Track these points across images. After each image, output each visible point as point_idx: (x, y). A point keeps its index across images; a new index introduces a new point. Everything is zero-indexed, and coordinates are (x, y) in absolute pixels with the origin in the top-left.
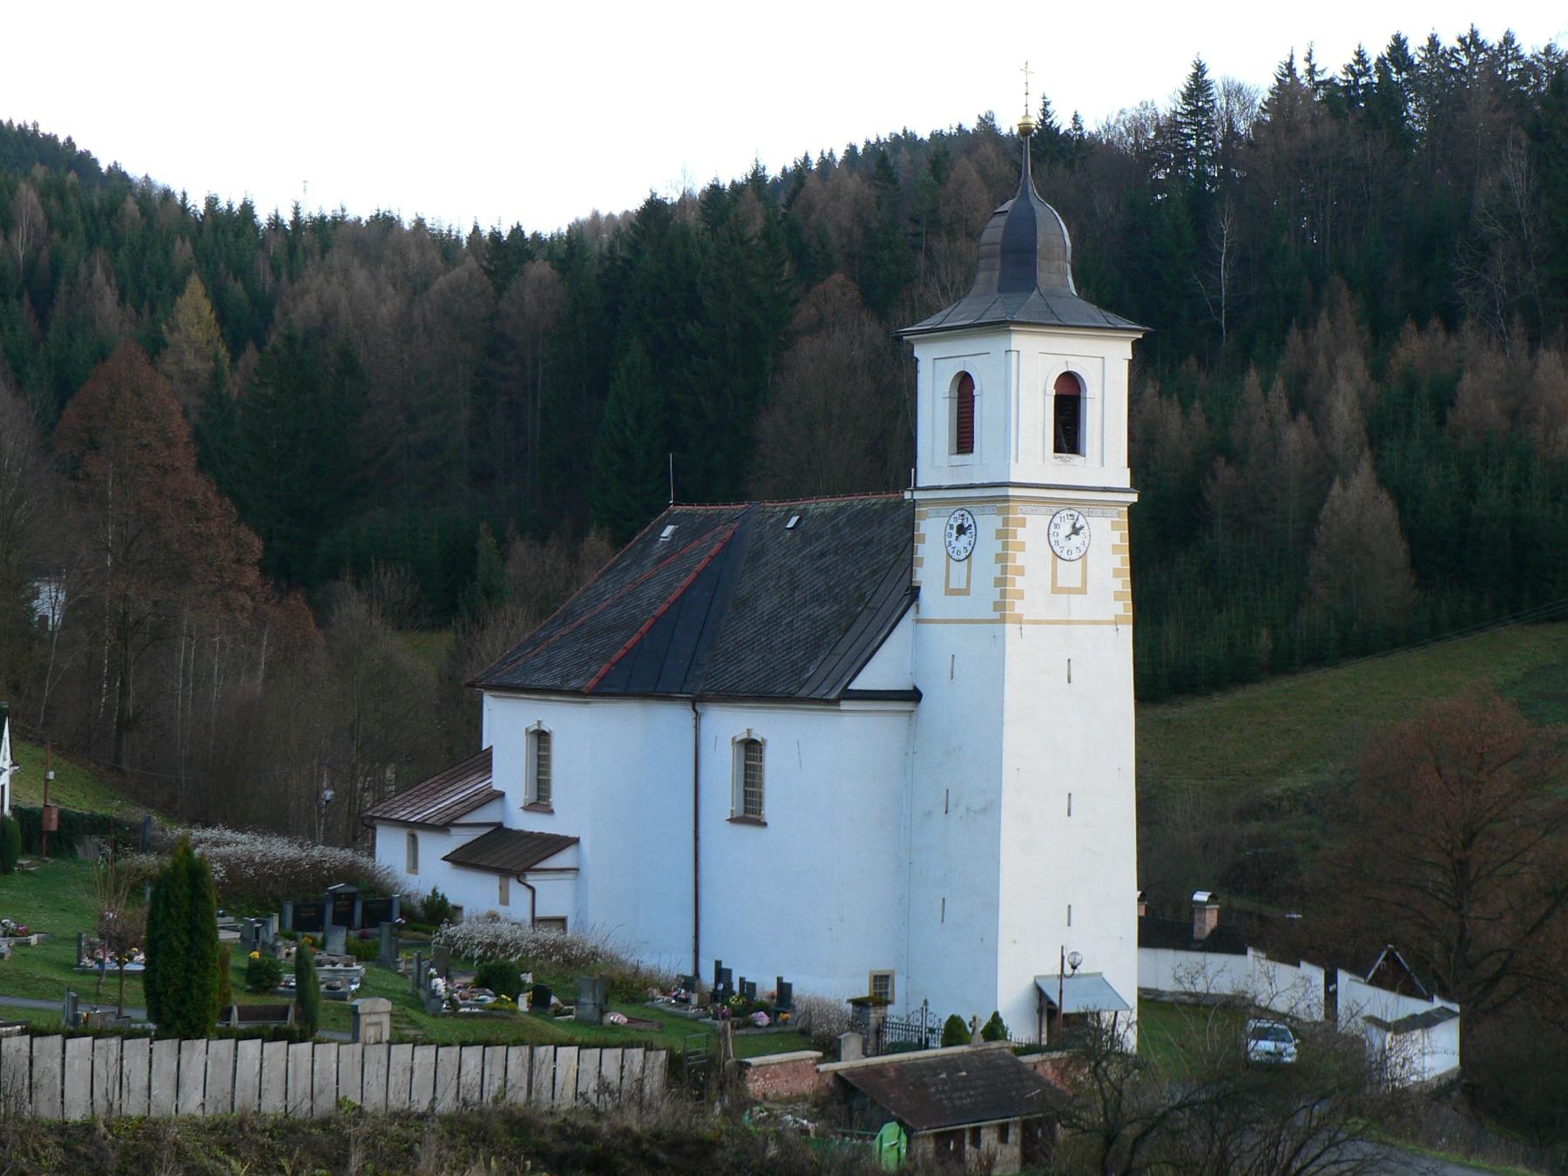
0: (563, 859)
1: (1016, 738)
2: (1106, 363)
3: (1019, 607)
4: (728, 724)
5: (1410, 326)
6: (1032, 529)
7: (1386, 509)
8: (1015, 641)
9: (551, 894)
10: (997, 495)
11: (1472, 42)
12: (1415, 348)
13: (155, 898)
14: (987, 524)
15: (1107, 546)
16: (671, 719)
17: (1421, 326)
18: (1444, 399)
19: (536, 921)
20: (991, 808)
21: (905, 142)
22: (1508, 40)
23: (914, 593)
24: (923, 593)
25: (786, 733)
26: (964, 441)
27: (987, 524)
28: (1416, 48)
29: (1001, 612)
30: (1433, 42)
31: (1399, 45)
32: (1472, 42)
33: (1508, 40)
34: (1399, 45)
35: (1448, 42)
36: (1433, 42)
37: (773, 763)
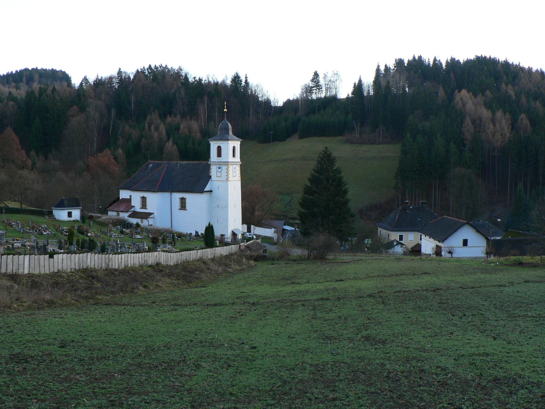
0: (152, 216)
1: (230, 197)
2: (237, 144)
3: (229, 179)
4: (177, 196)
5: (169, 116)
6: (231, 168)
7: (175, 147)
8: (230, 184)
9: (151, 221)
10: (227, 163)
11: (161, 66)
12: (169, 119)
13: (266, 243)
14: (224, 167)
15: (238, 168)
16: (167, 195)
17: (170, 116)
18: (178, 128)
19: (149, 225)
20: (227, 207)
21: (26, 70)
22: (166, 66)
23: (211, 177)
24: (212, 177)
25: (190, 198)
26: (219, 155)
27: (224, 167)
28: (153, 67)
29: (227, 180)
30: (155, 66)
31: (150, 66)
32: (161, 66)
33: (166, 66)
34: (150, 66)
35: (158, 66)
36: (155, 66)
37: (187, 201)
